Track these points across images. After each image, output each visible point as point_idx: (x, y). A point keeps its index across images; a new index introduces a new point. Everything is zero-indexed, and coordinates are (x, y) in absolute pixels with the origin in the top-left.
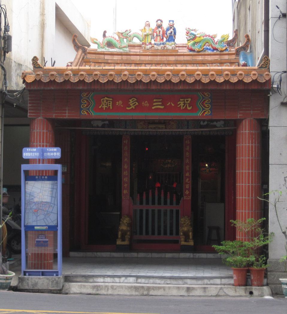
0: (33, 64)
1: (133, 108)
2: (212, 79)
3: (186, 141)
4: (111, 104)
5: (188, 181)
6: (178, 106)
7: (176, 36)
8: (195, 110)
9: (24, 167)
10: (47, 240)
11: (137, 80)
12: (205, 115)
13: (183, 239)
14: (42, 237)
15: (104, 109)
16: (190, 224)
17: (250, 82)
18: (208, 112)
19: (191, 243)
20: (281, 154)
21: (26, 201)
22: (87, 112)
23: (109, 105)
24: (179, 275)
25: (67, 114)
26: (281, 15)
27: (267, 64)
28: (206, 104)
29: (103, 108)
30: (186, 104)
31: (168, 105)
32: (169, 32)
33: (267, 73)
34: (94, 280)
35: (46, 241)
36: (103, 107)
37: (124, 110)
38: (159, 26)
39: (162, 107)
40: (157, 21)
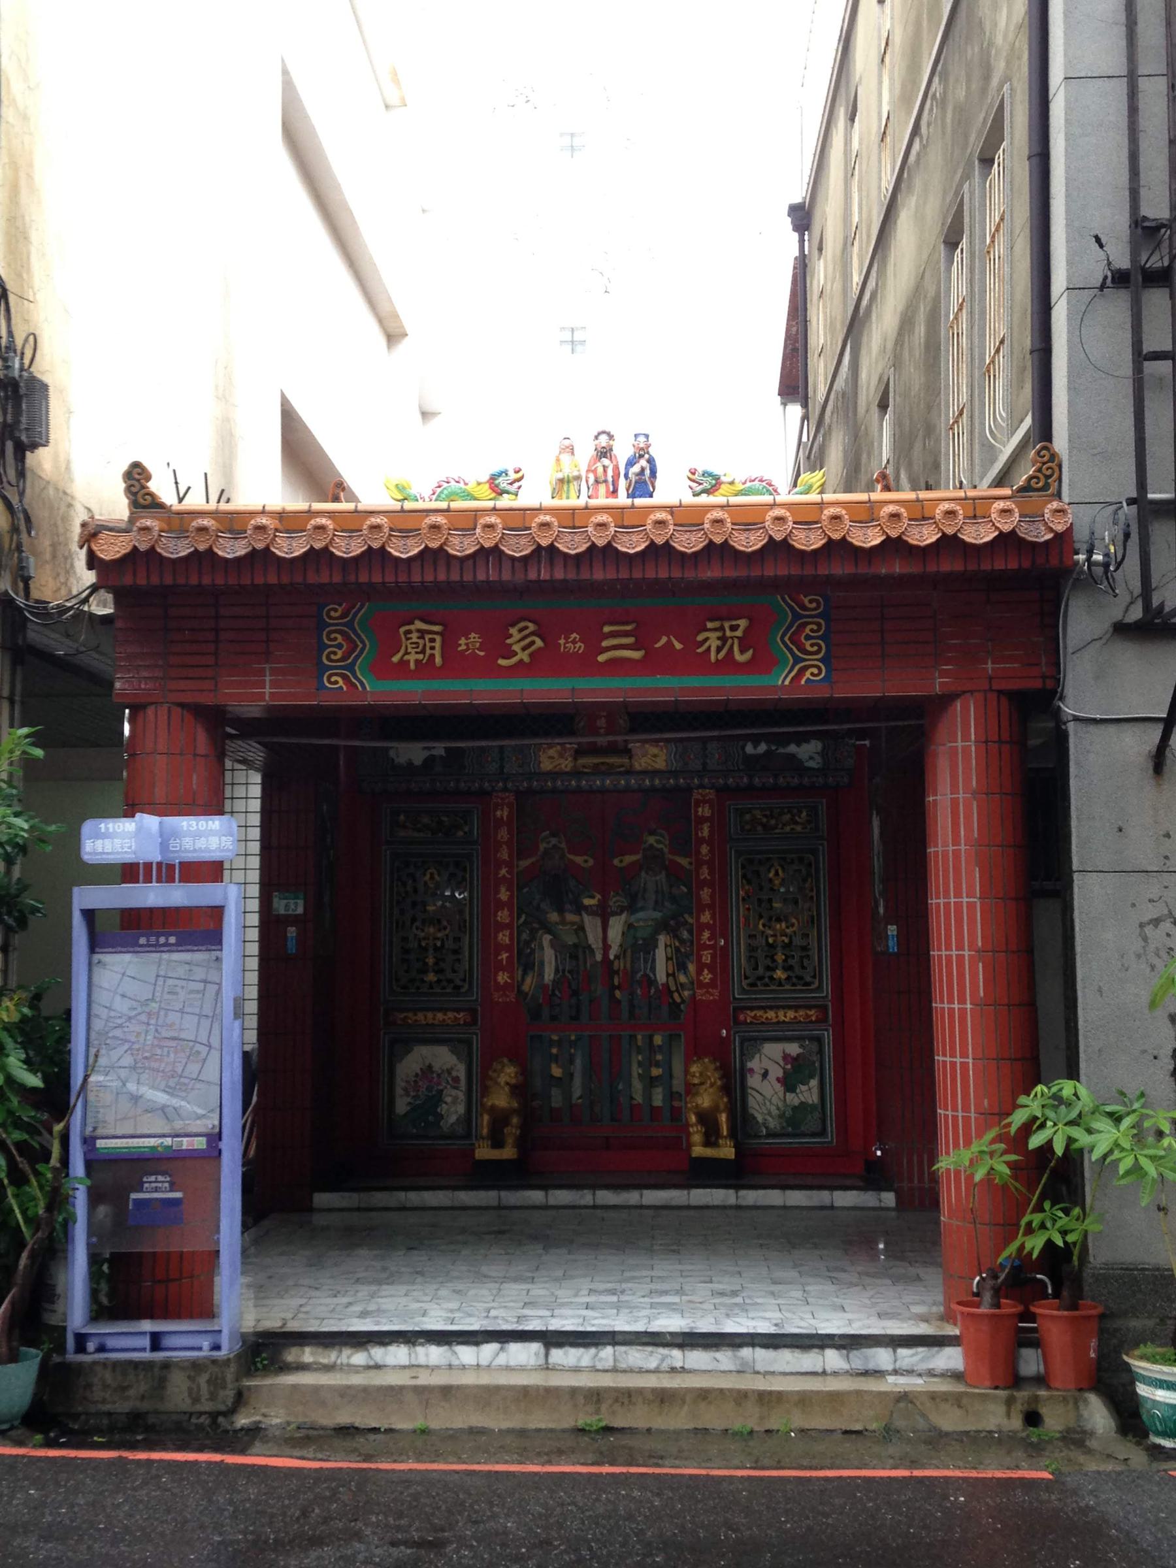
0: (129, 490)
1: (521, 661)
2: (836, 536)
3: (700, 809)
4: (438, 645)
5: (709, 939)
6: (700, 650)
7: (657, 484)
8: (763, 662)
9: (87, 897)
10: (178, 1195)
11: (539, 546)
12: (803, 682)
13: (697, 1138)
14: (160, 1185)
15: (412, 666)
16: (719, 1083)
17: (986, 544)
18: (816, 671)
19: (727, 1151)
20: (1120, 830)
21: (93, 1035)
22: (344, 677)
23: (428, 652)
24: (717, 1323)
25: (267, 690)
26: (1109, 274)
27: (1050, 476)
28: (808, 638)
29: (409, 661)
30: (730, 641)
31: (657, 646)
32: (636, 469)
33: (1055, 505)
34: (370, 1356)
35: (174, 1199)
36: (406, 657)
37: (489, 669)
38: (604, 453)
39: (636, 655)
40: (596, 438)
